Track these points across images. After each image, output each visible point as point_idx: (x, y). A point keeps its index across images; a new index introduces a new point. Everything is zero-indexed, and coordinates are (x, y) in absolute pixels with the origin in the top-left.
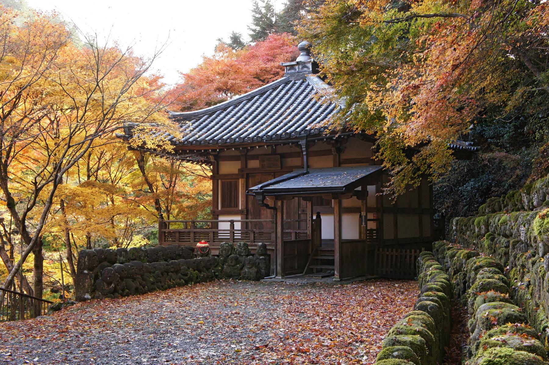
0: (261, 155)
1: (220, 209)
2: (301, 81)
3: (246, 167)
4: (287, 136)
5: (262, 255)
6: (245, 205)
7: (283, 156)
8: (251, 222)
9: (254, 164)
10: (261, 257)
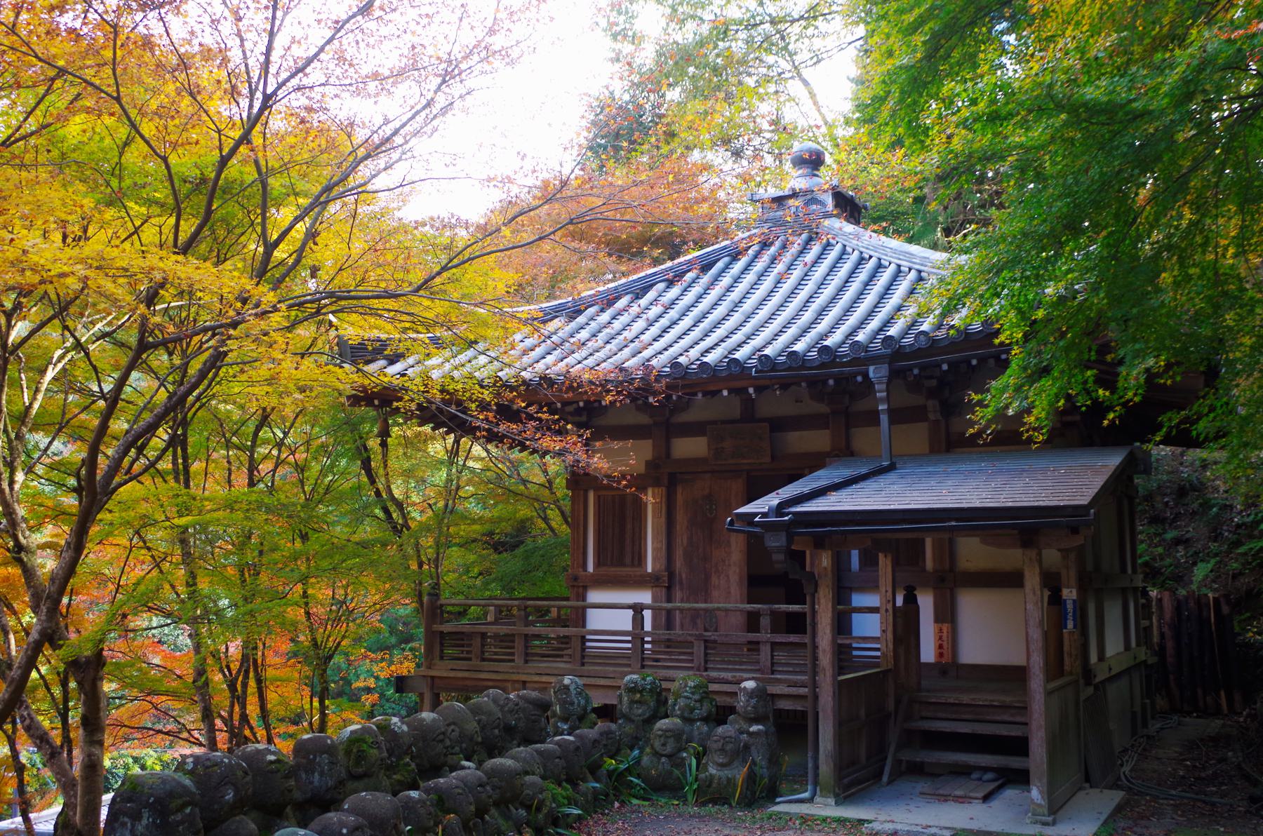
0: (714, 422)
1: (591, 568)
2: (804, 236)
3: (668, 455)
4: (826, 358)
5: (756, 720)
6: (664, 561)
7: (779, 425)
8: (681, 610)
9: (690, 447)
10: (754, 728)
